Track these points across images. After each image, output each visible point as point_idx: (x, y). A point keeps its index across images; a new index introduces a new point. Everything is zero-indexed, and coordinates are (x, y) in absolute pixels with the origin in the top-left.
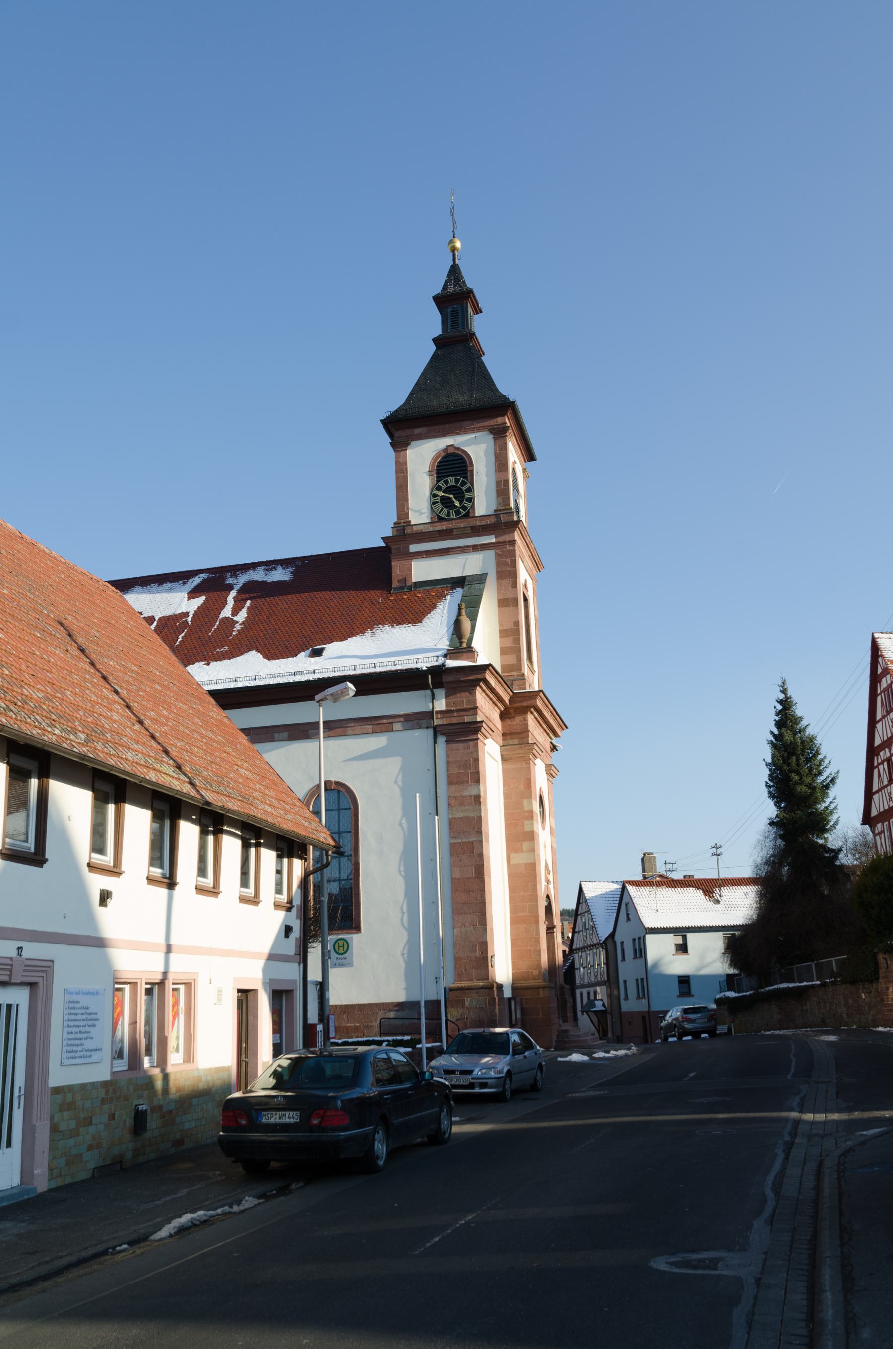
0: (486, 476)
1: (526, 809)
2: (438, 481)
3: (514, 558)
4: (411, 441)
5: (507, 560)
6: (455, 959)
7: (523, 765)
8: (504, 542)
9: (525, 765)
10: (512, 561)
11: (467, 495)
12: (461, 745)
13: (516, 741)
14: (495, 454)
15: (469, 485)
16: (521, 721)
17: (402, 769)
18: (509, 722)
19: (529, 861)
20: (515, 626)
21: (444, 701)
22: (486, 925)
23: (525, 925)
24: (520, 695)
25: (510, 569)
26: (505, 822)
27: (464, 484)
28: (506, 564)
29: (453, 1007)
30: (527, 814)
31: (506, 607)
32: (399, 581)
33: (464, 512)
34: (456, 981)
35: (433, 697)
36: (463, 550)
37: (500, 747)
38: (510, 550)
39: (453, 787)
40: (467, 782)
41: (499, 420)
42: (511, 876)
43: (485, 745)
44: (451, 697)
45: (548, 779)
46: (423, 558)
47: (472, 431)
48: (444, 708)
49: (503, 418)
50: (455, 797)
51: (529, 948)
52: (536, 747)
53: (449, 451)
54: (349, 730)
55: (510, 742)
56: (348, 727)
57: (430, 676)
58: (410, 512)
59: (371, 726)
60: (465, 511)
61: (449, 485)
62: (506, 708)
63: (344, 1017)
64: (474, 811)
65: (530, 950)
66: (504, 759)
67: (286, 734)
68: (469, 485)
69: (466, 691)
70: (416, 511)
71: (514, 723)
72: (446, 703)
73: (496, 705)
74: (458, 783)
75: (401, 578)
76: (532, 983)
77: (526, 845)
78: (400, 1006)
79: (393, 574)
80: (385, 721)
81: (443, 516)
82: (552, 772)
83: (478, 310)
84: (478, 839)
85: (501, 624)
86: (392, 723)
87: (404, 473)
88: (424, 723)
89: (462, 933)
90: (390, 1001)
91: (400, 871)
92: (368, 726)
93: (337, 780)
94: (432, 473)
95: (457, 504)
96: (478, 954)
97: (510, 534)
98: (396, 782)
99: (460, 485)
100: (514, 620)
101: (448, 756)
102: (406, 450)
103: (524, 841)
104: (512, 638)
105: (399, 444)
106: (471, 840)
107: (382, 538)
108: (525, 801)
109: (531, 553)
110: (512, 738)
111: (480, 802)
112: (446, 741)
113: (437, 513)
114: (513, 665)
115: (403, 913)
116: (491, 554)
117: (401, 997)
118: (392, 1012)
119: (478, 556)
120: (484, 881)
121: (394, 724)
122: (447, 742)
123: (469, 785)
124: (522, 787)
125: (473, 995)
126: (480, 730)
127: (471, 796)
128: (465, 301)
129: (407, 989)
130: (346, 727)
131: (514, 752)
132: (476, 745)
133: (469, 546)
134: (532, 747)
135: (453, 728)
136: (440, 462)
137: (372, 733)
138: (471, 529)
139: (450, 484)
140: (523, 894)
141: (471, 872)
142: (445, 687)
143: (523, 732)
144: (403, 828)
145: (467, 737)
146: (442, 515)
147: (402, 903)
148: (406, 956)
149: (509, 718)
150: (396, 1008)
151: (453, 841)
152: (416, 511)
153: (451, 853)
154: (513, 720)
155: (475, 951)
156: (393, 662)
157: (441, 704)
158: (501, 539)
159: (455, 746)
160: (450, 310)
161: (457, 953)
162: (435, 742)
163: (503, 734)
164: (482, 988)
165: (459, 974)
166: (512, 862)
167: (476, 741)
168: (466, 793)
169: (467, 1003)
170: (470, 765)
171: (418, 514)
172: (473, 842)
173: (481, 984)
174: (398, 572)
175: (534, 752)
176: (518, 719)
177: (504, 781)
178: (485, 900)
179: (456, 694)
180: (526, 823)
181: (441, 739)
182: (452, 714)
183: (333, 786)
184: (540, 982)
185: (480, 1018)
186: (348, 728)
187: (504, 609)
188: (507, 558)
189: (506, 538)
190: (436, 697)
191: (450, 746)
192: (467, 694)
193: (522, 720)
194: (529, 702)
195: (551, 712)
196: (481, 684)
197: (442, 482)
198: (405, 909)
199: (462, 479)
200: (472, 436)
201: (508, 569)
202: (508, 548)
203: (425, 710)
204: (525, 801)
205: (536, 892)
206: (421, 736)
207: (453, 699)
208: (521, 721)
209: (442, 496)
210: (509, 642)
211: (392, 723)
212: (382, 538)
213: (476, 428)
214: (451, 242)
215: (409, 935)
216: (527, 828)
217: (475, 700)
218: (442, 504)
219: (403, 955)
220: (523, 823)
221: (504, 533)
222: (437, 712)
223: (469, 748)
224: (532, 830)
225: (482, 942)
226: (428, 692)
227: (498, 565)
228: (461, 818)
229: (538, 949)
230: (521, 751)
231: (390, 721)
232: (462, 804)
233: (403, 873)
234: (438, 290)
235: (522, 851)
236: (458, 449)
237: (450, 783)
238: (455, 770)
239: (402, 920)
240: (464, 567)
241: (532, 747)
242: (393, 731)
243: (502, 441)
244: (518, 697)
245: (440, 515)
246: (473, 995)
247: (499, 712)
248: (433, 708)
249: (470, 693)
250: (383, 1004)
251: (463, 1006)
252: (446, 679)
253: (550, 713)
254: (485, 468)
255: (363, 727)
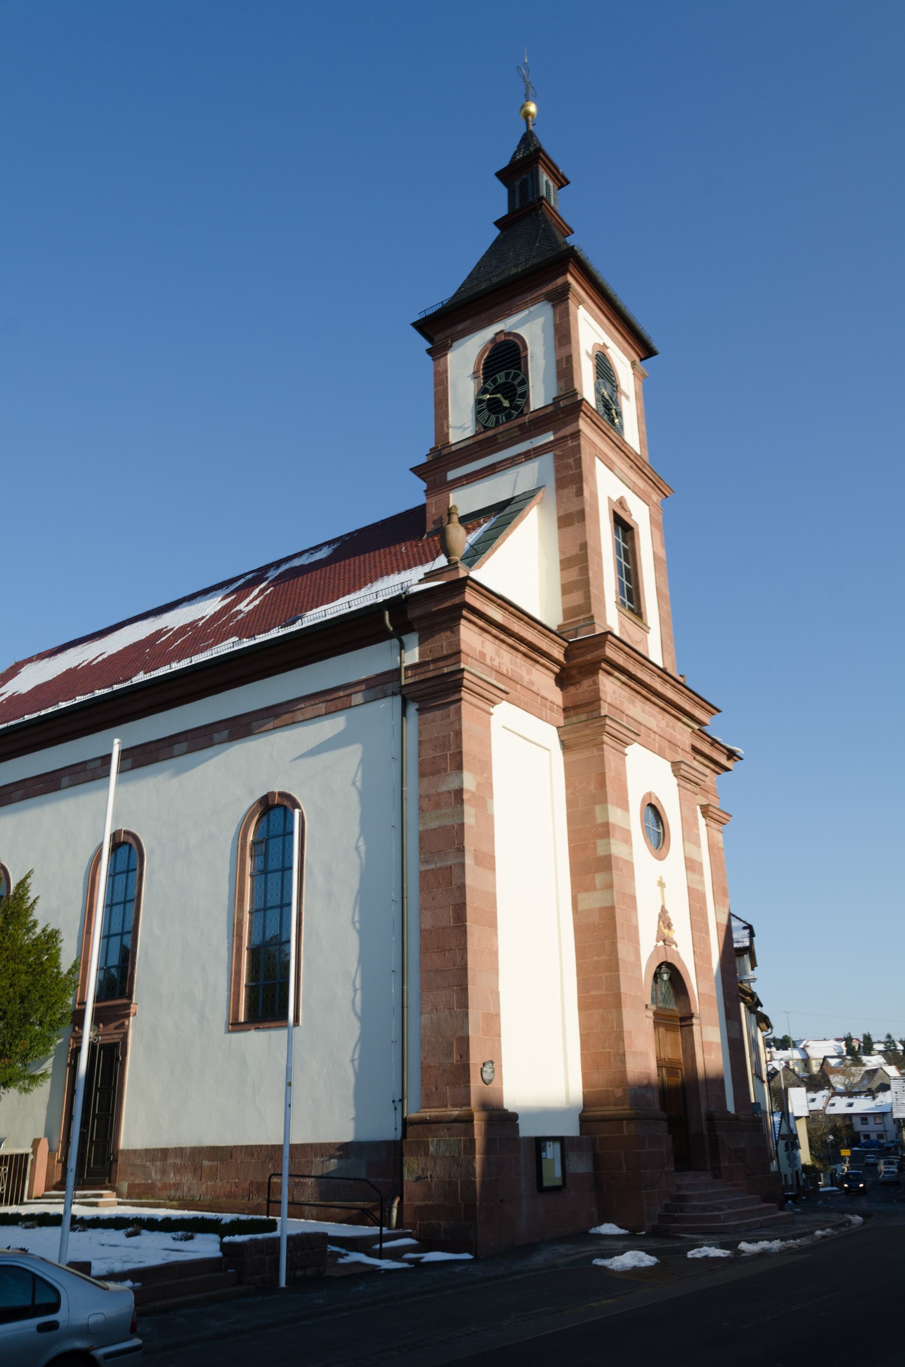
0: (545, 358)
1: (599, 820)
2: (485, 383)
3: (578, 456)
4: (453, 342)
5: (569, 460)
6: (422, 1068)
7: (593, 752)
8: (565, 437)
9: (596, 753)
10: (575, 461)
11: (520, 390)
12: (438, 714)
13: (583, 717)
14: (555, 326)
15: (522, 376)
16: (589, 686)
17: (363, 762)
18: (572, 690)
19: (605, 904)
20: (581, 550)
21: (416, 650)
22: (468, 1008)
23: (601, 1011)
24: (579, 644)
25: (574, 471)
26: (569, 844)
27: (516, 376)
28: (569, 467)
29: (411, 1155)
30: (600, 829)
31: (569, 525)
32: (434, 523)
33: (517, 413)
34: (422, 1108)
35: (402, 647)
36: (513, 462)
37: (558, 728)
38: (573, 446)
39: (426, 780)
40: (445, 770)
41: (560, 281)
42: (578, 930)
43: (626, 755)
44: (426, 643)
45: (678, 785)
46: (463, 485)
47: (525, 306)
48: (416, 660)
49: (563, 277)
50: (427, 796)
51: (608, 1050)
52: (608, 721)
53: (498, 341)
54: (299, 716)
55: (575, 719)
56: (297, 710)
57: (387, 613)
58: (450, 430)
59: (325, 704)
60: (517, 411)
61: (498, 384)
62: (563, 669)
63: (270, 1166)
64: (453, 816)
65: (609, 1052)
66: (566, 746)
67: (226, 733)
68: (522, 376)
69: (446, 629)
70: (459, 428)
71: (580, 690)
72: (420, 652)
73: (537, 662)
74: (432, 774)
75: (436, 518)
76: (611, 1110)
77: (599, 879)
78: (344, 1150)
79: (428, 515)
80: (341, 694)
81: (490, 425)
82: (682, 772)
83: (562, 182)
84: (458, 861)
85: (562, 551)
86: (351, 694)
87: (444, 384)
88: (390, 688)
89: (432, 1023)
90: (333, 1141)
91: (353, 923)
92: (321, 705)
93: (281, 790)
94: (477, 375)
95: (506, 404)
96: (455, 1057)
97: (573, 424)
98: (354, 783)
99: (512, 380)
100: (579, 542)
101: (420, 733)
102: (446, 354)
103: (596, 872)
104: (577, 568)
105: (438, 351)
106: (448, 863)
107: (411, 470)
108: (598, 808)
109: (632, 461)
110: (577, 714)
111: (462, 800)
112: (417, 710)
113: (483, 423)
114: (579, 606)
115: (355, 991)
116: (548, 459)
117: (347, 1136)
118: (333, 1161)
119: (531, 465)
120: (465, 931)
121: (353, 696)
122: (420, 711)
123: (448, 775)
124: (592, 787)
125: (442, 1133)
126: (462, 686)
127: (449, 792)
128: (535, 166)
129: (358, 1120)
130: (295, 711)
131: (578, 735)
132: (459, 711)
133: (519, 455)
134: (602, 723)
135: (423, 687)
136: (488, 357)
137: (326, 714)
138: (520, 430)
139: (500, 381)
140: (596, 958)
141: (447, 918)
142: (416, 627)
143: (592, 703)
144: (359, 853)
145: (446, 699)
146: (489, 425)
147: (354, 974)
148: (356, 1062)
149: (573, 684)
150: (338, 1154)
151: (424, 867)
152: (459, 428)
153: (420, 887)
154: (578, 686)
155: (451, 1054)
156: (347, 604)
157: (412, 656)
158: (561, 434)
159: (429, 716)
160: (517, 183)
161: (425, 1058)
162: (404, 714)
163: (565, 710)
164: (457, 1120)
165: (427, 1095)
166: (580, 908)
167: (458, 704)
168: (443, 788)
169: (431, 1148)
170: (449, 742)
171: (461, 430)
172: (451, 867)
173: (456, 1112)
174: (434, 511)
175: (608, 729)
176: (586, 684)
177: (567, 780)
178: (466, 964)
179: (433, 636)
180: (600, 842)
181: (412, 709)
182: (426, 668)
183: (277, 800)
184: (624, 1110)
185: (450, 1177)
186: (298, 712)
187: (565, 529)
188: (568, 459)
189: (568, 430)
190: (407, 647)
191: (424, 716)
192: (448, 633)
193: (592, 684)
194: (594, 654)
195: (659, 676)
196: (464, 613)
197: (489, 382)
198: (358, 986)
199: (513, 371)
200: (526, 312)
201: (570, 472)
202: (570, 444)
203: (391, 669)
204: (598, 808)
205: (617, 955)
206: (389, 706)
207: (430, 644)
208: (589, 686)
209: (489, 399)
210: (573, 574)
211: (351, 694)
212: (411, 470)
213: (531, 300)
214: (523, 106)
215: (363, 1029)
216: (601, 852)
217: (459, 640)
218: (489, 410)
219: (353, 1061)
220: (595, 844)
221: (565, 425)
222: (407, 668)
223: (449, 716)
224: (607, 853)
225: (462, 1038)
226: (395, 642)
227: (558, 470)
228: (435, 829)
229: (621, 1052)
230: (588, 731)
231: (348, 692)
232: (437, 806)
233: (357, 925)
234: (504, 163)
235: (594, 889)
236: (509, 334)
237: (422, 775)
238: (431, 754)
239: (353, 1003)
240: (515, 485)
241: (602, 723)
242: (351, 707)
243: (563, 306)
244: (578, 649)
245: (486, 425)
246: (442, 1133)
247: (553, 676)
248: (401, 662)
249: (453, 632)
250: (321, 1145)
251: (426, 1154)
252: (414, 613)
253: (659, 680)
254: (543, 348)
255: (315, 707)
